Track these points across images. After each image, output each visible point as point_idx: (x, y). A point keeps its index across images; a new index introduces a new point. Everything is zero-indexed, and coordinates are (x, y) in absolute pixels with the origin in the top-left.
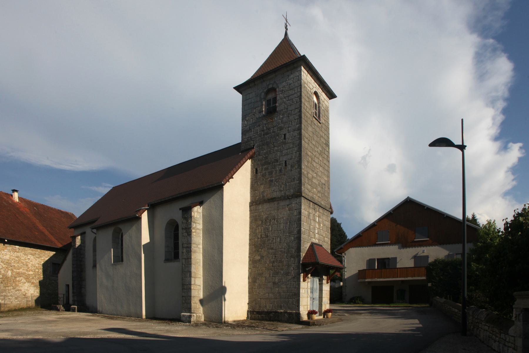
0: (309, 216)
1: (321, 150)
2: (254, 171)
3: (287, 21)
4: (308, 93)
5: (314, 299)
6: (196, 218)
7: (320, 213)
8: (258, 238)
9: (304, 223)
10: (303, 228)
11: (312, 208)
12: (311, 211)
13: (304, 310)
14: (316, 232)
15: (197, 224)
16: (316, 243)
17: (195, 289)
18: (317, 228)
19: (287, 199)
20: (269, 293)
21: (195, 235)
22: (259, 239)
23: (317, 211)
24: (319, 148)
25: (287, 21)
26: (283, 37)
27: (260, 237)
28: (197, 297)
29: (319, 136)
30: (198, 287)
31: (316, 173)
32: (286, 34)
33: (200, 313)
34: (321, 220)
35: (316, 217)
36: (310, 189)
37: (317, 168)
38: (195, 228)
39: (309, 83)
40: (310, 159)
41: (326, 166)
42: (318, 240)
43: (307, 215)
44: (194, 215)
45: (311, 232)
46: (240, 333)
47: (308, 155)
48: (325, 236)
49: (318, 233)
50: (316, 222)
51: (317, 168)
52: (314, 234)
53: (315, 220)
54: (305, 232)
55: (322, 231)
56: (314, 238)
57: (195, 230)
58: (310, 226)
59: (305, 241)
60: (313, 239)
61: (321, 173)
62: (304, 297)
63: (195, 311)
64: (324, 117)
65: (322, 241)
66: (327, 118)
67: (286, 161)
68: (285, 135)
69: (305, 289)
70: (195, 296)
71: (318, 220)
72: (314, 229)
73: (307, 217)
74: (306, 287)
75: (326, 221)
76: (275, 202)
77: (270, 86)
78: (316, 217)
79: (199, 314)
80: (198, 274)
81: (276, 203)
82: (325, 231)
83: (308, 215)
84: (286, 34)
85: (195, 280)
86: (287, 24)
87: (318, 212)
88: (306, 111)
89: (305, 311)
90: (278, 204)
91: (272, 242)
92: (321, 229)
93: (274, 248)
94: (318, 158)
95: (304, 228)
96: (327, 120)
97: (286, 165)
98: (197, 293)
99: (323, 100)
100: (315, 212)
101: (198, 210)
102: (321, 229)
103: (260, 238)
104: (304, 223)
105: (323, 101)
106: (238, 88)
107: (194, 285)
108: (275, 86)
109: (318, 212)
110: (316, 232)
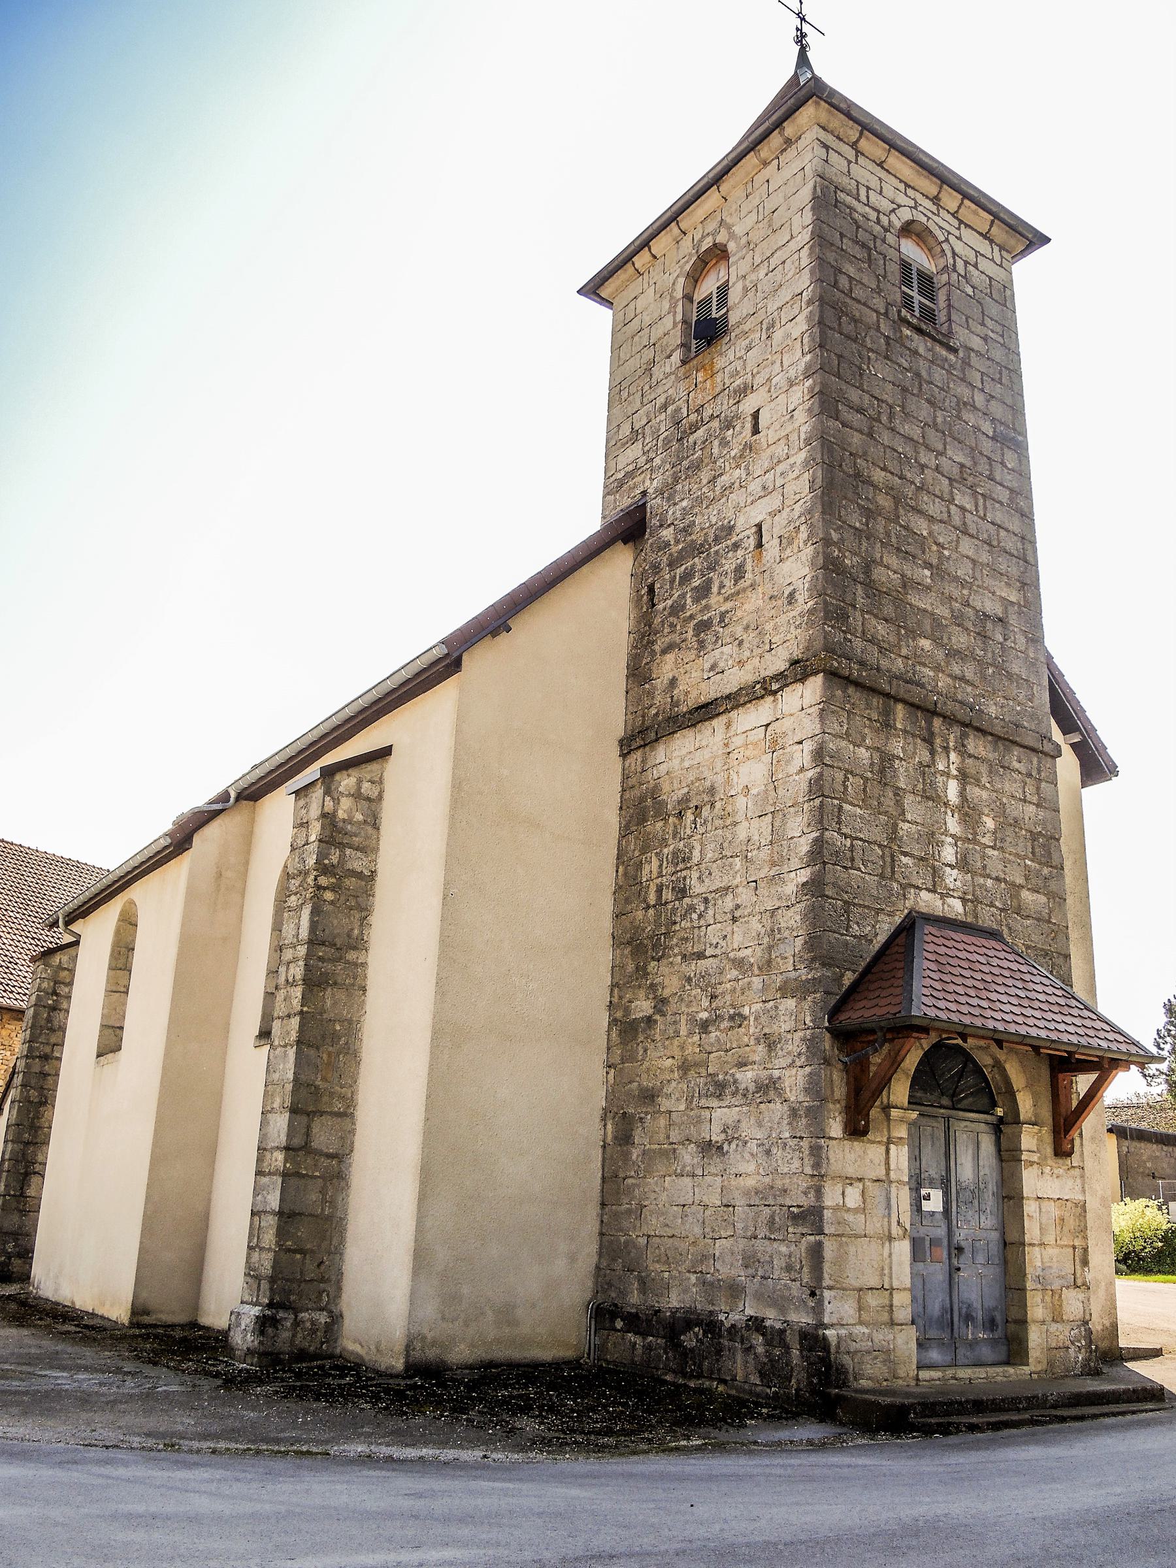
0: (882, 771)
1: (968, 463)
2: (642, 596)
3: (803, 19)
4: (858, 227)
5: (960, 1249)
6: (344, 821)
7: (970, 761)
8: (648, 907)
9: (847, 807)
10: (839, 832)
11: (905, 731)
12: (897, 747)
13: (861, 1323)
14: (949, 854)
15: (348, 851)
16: (952, 916)
17: (304, 1176)
18: (953, 836)
19: (762, 697)
20: (684, 1206)
21: (332, 903)
22: (651, 911)
23: (946, 749)
24: (949, 453)
25: (803, 19)
26: (789, 71)
27: (652, 903)
28: (311, 1215)
29: (950, 402)
30: (325, 1162)
31: (928, 565)
32: (803, 60)
33: (322, 1309)
34: (974, 792)
35: (940, 779)
36: (892, 639)
37: (938, 544)
38: (338, 871)
39: (868, 188)
40: (885, 502)
41: (1003, 533)
42: (964, 901)
43: (872, 764)
44: (335, 811)
45: (906, 854)
46: (867, 1396)
47: (869, 482)
48: (1020, 881)
49: (963, 864)
50: (946, 804)
51: (938, 544)
52: (933, 867)
53: (932, 796)
54: (858, 855)
55: (990, 852)
56: (934, 891)
57: (333, 880)
58: (895, 825)
59: (855, 905)
60: (924, 895)
61: (971, 566)
62: (857, 1236)
63: (293, 1298)
64: (983, 324)
65: (1002, 910)
66: (999, 329)
67: (759, 526)
68: (756, 416)
69: (868, 1183)
70: (300, 1214)
71: (962, 794)
72: (931, 838)
73: (866, 780)
74: (873, 1175)
75: (1025, 801)
76: (715, 722)
77: (707, 244)
78: (940, 779)
79: (316, 1315)
80: (332, 1095)
81: (718, 723)
82: (1017, 855)
83: (876, 768)
84: (803, 60)
85: (879, 1142)
86: (806, 28)
87: (953, 756)
88: (854, 299)
89: (866, 1325)
90: (728, 725)
91: (702, 922)
92: (987, 840)
93: (707, 954)
94: (946, 497)
95: (844, 831)
96: (1000, 340)
97: (760, 545)
98: (314, 1196)
99: (971, 257)
100: (933, 753)
101: (359, 788)
102: (987, 840)
103: (654, 906)
104: (847, 807)
105: (966, 263)
106: (593, 289)
107: (301, 1153)
108: (721, 238)
109: (953, 756)
110: (949, 854)
